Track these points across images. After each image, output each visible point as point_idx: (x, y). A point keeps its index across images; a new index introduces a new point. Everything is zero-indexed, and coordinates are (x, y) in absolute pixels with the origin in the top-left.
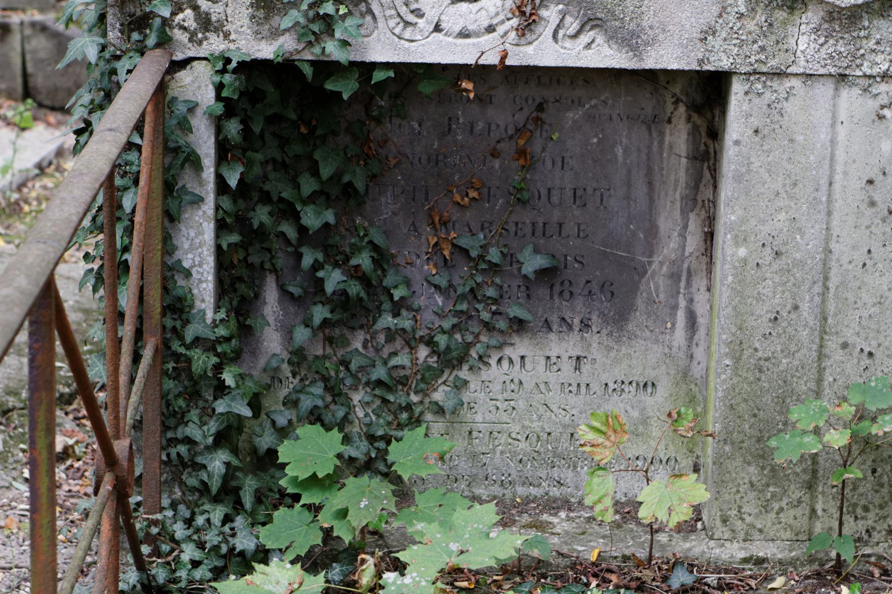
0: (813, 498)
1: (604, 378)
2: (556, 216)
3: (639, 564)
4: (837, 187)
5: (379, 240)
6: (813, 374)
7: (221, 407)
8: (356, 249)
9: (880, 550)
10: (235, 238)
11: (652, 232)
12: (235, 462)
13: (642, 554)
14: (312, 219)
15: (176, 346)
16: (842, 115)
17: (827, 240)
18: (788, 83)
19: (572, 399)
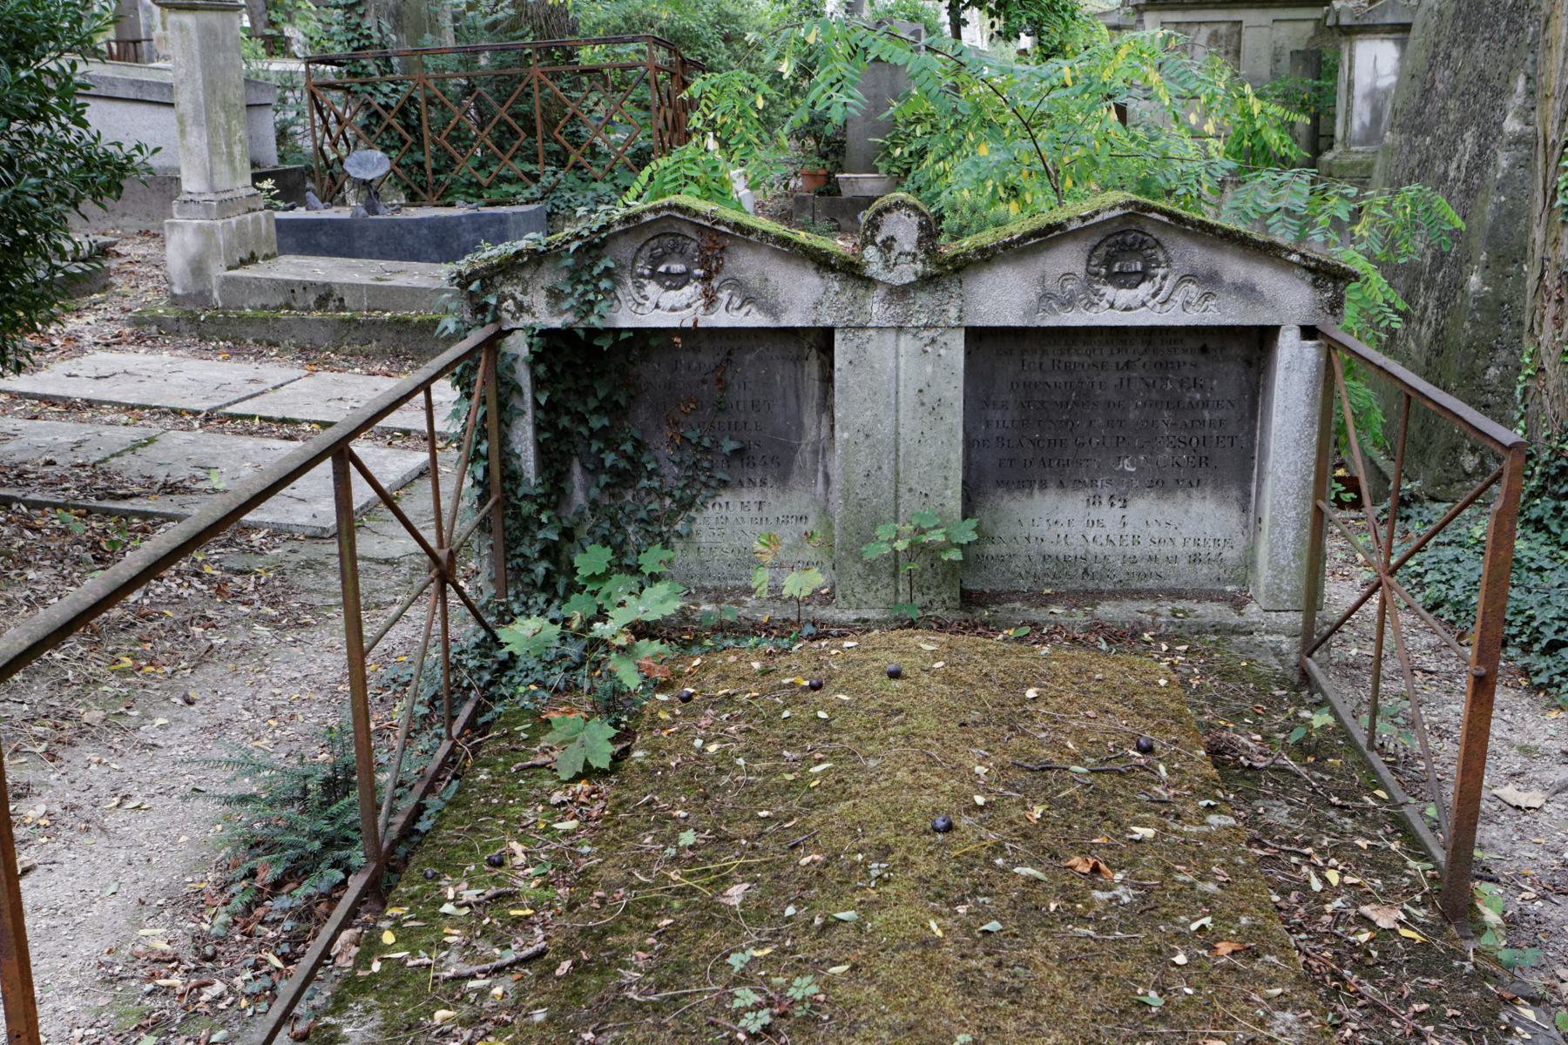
0: (897, 583)
1: (777, 514)
2: (743, 417)
3: (793, 624)
4: (901, 395)
5: (637, 435)
6: (892, 508)
7: (540, 535)
8: (624, 441)
9: (938, 613)
10: (547, 435)
11: (800, 426)
12: (552, 568)
13: (794, 618)
14: (597, 422)
15: (513, 500)
16: (902, 351)
17: (897, 426)
18: (868, 333)
19: (758, 528)
